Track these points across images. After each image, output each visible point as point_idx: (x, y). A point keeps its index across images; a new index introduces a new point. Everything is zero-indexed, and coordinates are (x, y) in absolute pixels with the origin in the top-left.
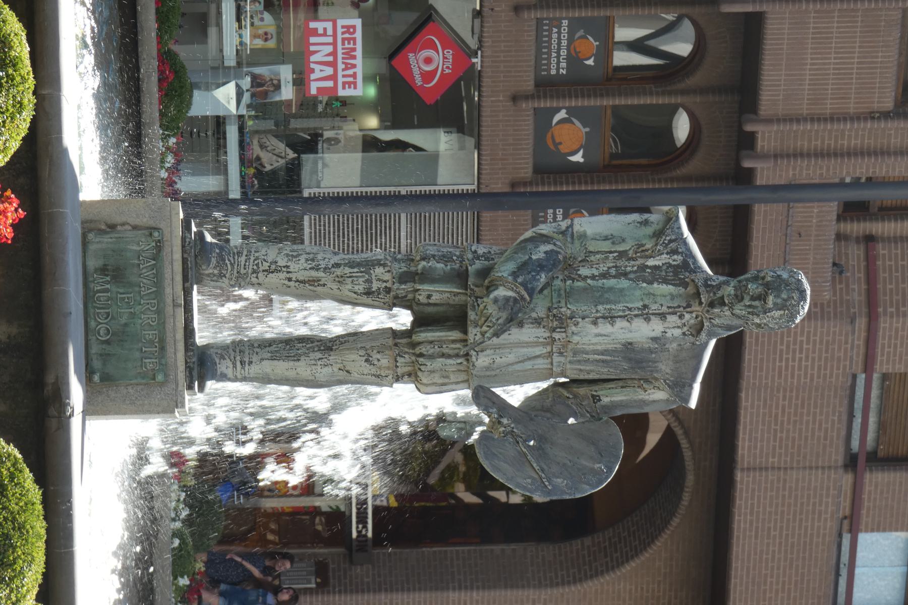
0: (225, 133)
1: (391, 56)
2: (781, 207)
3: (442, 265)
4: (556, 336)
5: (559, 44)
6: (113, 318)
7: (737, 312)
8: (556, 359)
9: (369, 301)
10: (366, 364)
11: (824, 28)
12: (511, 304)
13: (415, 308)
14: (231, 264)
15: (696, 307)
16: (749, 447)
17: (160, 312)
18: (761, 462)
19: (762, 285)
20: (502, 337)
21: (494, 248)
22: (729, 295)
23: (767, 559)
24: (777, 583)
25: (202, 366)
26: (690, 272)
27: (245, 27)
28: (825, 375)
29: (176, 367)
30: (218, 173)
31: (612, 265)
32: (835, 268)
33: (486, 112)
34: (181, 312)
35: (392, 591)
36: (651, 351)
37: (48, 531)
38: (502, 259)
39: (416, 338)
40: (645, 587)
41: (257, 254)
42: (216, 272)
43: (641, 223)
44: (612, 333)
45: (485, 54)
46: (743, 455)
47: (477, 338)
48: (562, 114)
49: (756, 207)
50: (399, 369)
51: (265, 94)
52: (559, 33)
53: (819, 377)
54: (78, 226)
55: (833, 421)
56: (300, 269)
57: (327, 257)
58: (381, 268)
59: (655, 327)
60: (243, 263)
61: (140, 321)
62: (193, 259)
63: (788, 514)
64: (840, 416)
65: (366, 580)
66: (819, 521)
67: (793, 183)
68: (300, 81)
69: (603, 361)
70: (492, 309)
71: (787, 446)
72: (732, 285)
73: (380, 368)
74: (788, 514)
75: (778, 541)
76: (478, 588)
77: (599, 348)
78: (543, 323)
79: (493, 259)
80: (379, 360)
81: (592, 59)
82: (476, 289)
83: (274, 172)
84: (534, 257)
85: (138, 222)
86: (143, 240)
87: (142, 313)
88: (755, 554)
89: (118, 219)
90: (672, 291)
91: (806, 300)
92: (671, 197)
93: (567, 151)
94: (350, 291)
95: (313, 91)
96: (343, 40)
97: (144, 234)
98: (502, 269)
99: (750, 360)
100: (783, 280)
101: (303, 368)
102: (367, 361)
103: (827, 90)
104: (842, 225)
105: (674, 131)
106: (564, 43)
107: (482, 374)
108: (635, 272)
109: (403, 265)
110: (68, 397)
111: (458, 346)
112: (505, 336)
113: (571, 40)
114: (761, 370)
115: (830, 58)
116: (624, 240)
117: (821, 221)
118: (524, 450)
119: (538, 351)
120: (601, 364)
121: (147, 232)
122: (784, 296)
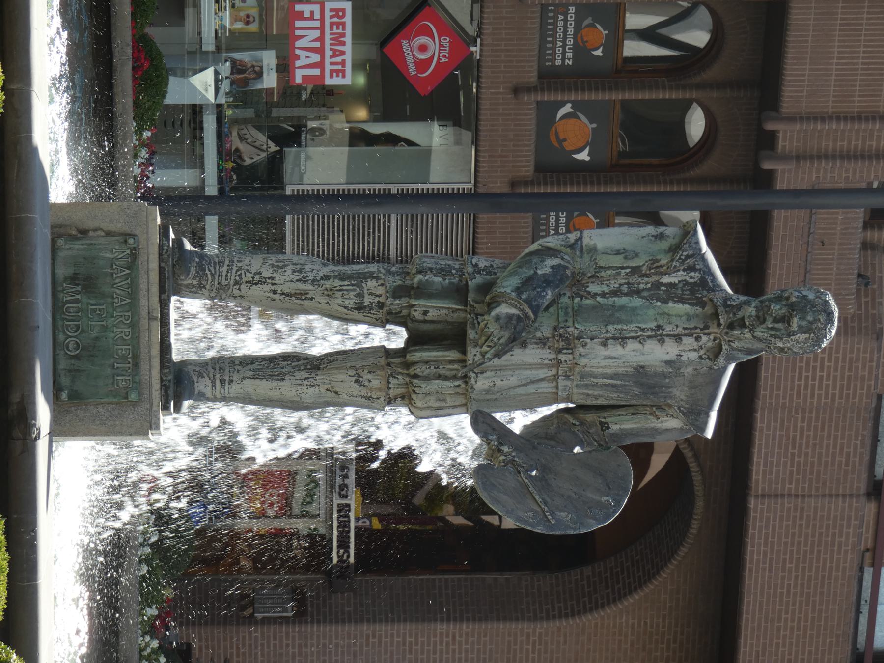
0: (202, 122)
1: (383, 44)
2: (803, 213)
3: (440, 279)
4: (563, 357)
5: (565, 32)
6: (83, 331)
7: (758, 334)
8: (562, 382)
9: (360, 316)
10: (355, 385)
11: (853, 19)
12: (514, 322)
13: (409, 324)
14: (212, 274)
15: (714, 329)
16: (764, 472)
17: (134, 325)
18: (776, 489)
19: (785, 305)
20: (504, 358)
21: (497, 261)
22: (750, 316)
23: (782, 594)
24: (793, 621)
25: (181, 384)
26: (708, 291)
27: (225, 9)
28: (848, 395)
29: (151, 385)
30: (194, 167)
31: (624, 281)
32: (861, 280)
33: (485, 104)
34: (156, 326)
35: (375, 621)
36: (664, 375)
37: (10, 563)
38: (505, 274)
39: (410, 357)
40: (648, 621)
41: (239, 264)
42: (195, 282)
43: (656, 237)
44: (623, 355)
45: (485, 42)
46: (757, 481)
47: (477, 359)
48: (567, 109)
49: (776, 213)
50: (391, 391)
51: (246, 82)
52: (565, 21)
53: (841, 398)
54: (48, 232)
55: (856, 445)
56: (286, 280)
57: (316, 268)
58: (374, 281)
59: (669, 349)
60: (224, 274)
61: (112, 335)
62: (171, 268)
63: (806, 545)
64: (863, 440)
65: (347, 609)
66: (839, 553)
67: (816, 187)
68: (284, 68)
69: (613, 386)
70: (493, 328)
71: (805, 471)
72: (754, 305)
73: (371, 390)
74: (806, 545)
75: (793, 574)
76: (468, 620)
77: (609, 371)
78: (548, 344)
79: (495, 273)
80: (370, 381)
82: (476, 305)
83: (254, 166)
84: (539, 272)
85: (111, 227)
86: (117, 247)
87: (114, 326)
88: (769, 588)
89: (90, 224)
90: (688, 310)
91: (833, 323)
92: (682, 201)
94: (340, 305)
95: (298, 80)
96: (332, 24)
97: (118, 241)
98: (505, 284)
99: (766, 377)
100: (809, 301)
101: (287, 388)
102: (357, 381)
103: (855, 86)
104: (869, 233)
105: (686, 127)
106: (571, 31)
107: (481, 397)
108: (649, 290)
109: (398, 278)
110: (35, 418)
111: (456, 366)
112: (507, 357)
113: (577, 29)
114: (779, 389)
115: (859, 52)
116: (637, 255)
117: (846, 229)
118: (526, 481)
119: (543, 373)
120: (610, 389)
121: (121, 239)
122: (810, 318)
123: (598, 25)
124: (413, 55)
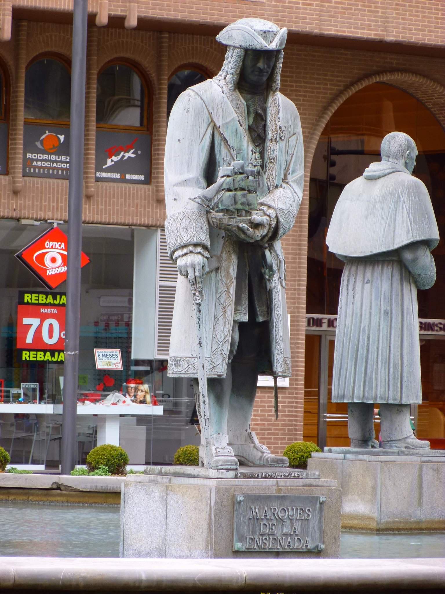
5: (46, 160)
16: (369, 30)
45: (51, 217)
46: (375, 35)
52: (37, 160)
81: (60, 136)
93: (58, 143)
106: (46, 157)
113: (43, 152)
123: (41, 139)
124: (58, 267)
